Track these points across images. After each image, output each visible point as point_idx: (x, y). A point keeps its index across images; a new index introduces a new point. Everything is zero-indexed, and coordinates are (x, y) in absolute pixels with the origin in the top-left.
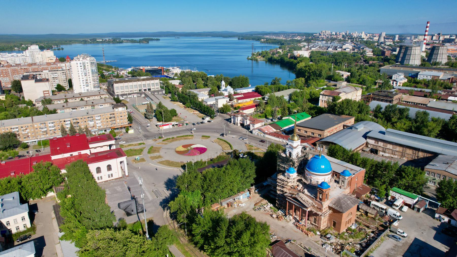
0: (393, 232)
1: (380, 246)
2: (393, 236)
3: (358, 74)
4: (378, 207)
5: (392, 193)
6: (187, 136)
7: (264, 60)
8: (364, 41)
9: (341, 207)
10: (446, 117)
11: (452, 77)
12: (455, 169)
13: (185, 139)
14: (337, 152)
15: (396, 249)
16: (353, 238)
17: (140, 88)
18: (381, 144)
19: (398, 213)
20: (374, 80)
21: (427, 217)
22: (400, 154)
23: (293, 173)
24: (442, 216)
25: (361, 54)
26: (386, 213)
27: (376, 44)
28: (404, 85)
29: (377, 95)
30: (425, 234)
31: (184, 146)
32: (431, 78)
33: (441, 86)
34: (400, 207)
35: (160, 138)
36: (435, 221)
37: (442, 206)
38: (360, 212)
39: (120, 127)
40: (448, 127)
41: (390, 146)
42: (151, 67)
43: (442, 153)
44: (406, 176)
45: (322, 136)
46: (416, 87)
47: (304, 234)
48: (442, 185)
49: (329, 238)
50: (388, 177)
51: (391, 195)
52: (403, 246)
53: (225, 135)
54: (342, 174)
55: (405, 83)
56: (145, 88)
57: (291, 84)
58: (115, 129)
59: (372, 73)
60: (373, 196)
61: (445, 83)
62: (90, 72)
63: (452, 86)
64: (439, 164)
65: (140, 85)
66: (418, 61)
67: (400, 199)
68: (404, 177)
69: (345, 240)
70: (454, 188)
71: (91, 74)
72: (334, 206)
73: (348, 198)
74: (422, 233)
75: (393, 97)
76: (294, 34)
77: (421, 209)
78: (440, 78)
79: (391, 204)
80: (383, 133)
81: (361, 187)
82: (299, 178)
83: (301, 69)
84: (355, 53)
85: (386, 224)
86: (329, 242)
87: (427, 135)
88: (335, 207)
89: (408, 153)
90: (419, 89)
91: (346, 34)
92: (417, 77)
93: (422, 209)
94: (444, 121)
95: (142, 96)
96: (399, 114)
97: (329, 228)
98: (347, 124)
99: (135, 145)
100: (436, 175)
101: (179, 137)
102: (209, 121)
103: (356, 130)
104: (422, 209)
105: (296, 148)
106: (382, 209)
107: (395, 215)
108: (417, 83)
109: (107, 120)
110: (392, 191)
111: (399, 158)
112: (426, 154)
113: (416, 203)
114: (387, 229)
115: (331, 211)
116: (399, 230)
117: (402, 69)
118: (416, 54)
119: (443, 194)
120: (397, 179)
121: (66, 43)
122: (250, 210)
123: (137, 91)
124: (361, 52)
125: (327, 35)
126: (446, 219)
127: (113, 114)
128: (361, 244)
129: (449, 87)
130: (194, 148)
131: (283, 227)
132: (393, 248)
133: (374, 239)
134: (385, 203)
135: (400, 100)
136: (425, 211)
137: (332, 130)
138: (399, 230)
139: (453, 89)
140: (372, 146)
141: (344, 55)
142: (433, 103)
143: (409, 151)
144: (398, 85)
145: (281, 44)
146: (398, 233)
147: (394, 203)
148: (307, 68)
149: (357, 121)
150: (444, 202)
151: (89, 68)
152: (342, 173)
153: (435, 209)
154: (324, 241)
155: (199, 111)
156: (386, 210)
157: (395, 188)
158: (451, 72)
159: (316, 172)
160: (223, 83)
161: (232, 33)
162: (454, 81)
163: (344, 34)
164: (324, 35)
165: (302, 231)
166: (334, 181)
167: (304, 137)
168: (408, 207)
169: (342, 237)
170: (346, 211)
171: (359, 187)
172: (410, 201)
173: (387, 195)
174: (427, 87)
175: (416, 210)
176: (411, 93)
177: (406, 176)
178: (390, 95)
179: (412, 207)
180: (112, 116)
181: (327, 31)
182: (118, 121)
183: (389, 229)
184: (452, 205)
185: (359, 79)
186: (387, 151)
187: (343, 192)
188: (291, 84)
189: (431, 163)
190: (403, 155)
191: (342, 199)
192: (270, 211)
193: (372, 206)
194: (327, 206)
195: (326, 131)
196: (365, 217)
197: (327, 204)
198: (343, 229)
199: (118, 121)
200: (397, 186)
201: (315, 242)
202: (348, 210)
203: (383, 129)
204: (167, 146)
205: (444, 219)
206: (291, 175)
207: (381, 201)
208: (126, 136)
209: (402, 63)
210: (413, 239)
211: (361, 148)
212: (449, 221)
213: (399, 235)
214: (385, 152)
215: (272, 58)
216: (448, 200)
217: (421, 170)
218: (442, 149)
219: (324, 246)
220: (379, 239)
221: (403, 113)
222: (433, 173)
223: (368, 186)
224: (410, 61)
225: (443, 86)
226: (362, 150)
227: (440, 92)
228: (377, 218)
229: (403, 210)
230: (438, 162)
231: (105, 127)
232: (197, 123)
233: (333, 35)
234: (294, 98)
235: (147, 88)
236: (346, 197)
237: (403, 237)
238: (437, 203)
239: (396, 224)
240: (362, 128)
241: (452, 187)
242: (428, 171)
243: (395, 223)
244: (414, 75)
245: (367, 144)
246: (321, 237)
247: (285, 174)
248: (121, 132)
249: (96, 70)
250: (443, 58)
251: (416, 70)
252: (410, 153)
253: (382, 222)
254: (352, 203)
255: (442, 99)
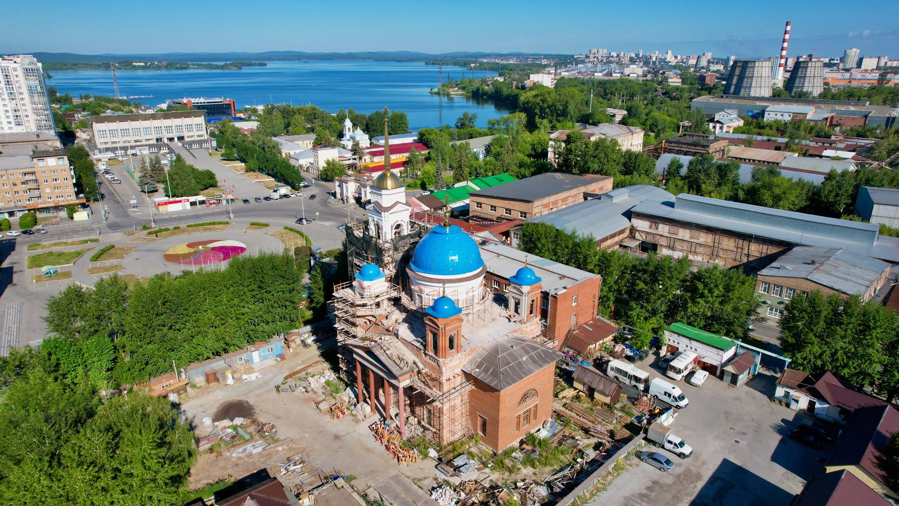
0: (653, 443)
1: (609, 488)
2: (652, 456)
3: (646, 111)
4: (625, 374)
5: (669, 338)
6: (214, 223)
7: (462, 95)
8: (671, 66)
9: (495, 374)
10: (818, 180)
11: (832, 115)
12: (831, 275)
13: (206, 229)
14: (539, 239)
15: (653, 495)
16: (533, 466)
17: (159, 136)
18: (664, 229)
19: (677, 388)
20: (676, 121)
21: (754, 398)
22: (708, 251)
23: (371, 280)
24: (793, 393)
25: (660, 83)
26: (647, 390)
27: (692, 70)
28: (737, 130)
29: (675, 143)
30: (743, 443)
31: (190, 246)
32: (790, 118)
33: (810, 133)
34: (685, 373)
35: (145, 228)
36: (775, 406)
37: (794, 365)
38: (575, 389)
39: (53, 205)
40: (821, 197)
41: (684, 234)
42: (206, 99)
43: (802, 243)
44: (706, 292)
45: (528, 215)
46: (759, 134)
47: (392, 455)
48: (795, 308)
49: (457, 469)
50: (663, 296)
51: (667, 342)
52: (675, 483)
53: (304, 222)
54: (514, 280)
55: (739, 127)
56: (171, 136)
57: (496, 126)
58: (41, 210)
59: (674, 110)
60: (619, 348)
61: (818, 128)
62: (25, 90)
63: (832, 132)
64: (793, 266)
65: (158, 128)
66: (767, 90)
67: (688, 353)
68: (702, 295)
69: (507, 473)
70: (824, 313)
71: (26, 96)
72: (476, 372)
73: (523, 348)
74: (737, 442)
75: (708, 146)
76: (537, 55)
77: (741, 377)
78: (808, 118)
79: (663, 366)
80: (671, 205)
81: (588, 325)
82: (394, 294)
83: (528, 102)
84: (647, 80)
85: (640, 422)
86: (456, 481)
87: (772, 207)
88: (480, 374)
89: (726, 247)
90: (765, 138)
91: (637, 55)
92: (763, 117)
93: (743, 378)
94: (811, 186)
95: (162, 152)
96: (717, 176)
97: (471, 437)
98: (594, 191)
99: (73, 244)
100: (784, 290)
101: (191, 226)
102: (286, 196)
103: (609, 201)
104: (743, 378)
105: (388, 209)
106: (637, 379)
107: (670, 395)
108: (763, 127)
109: (16, 189)
110: (669, 331)
111: (705, 260)
112: (765, 247)
113: (729, 361)
114: (637, 434)
115: (470, 387)
116: (671, 438)
117: (734, 102)
118: (763, 75)
119: (797, 336)
120: (685, 303)
121: (65, 67)
122: (267, 391)
123: (151, 142)
124: (660, 79)
125: (600, 58)
126: (803, 401)
127: (33, 173)
128: (549, 485)
129: (825, 134)
130: (214, 249)
131: (337, 437)
132: (645, 492)
133: (595, 464)
134: (652, 366)
135: (723, 154)
136: (753, 383)
137: (555, 203)
138: (670, 438)
139: (833, 138)
140: (644, 236)
141: (625, 82)
142: (791, 160)
143: (728, 243)
144: (724, 131)
145: (502, 70)
146: (667, 446)
147: (672, 363)
148: (538, 100)
149: (616, 186)
150: (799, 356)
151: (22, 83)
152: (514, 277)
153: (778, 375)
154: (442, 477)
155: (273, 177)
156: (646, 381)
157: (675, 326)
158: (830, 107)
159: (430, 272)
160: (348, 123)
161: (416, 54)
162: (834, 123)
163: (634, 55)
164: (595, 57)
165: (387, 448)
166: (491, 296)
167: (491, 220)
168: (707, 373)
169: (500, 465)
170: (509, 384)
171: (586, 324)
172: (714, 358)
173: (656, 344)
174: (782, 135)
175: (727, 378)
176: (749, 144)
177: (706, 292)
178: (702, 142)
179: (718, 373)
180: (28, 177)
181: (600, 50)
182: (48, 190)
183: (642, 435)
184: (819, 363)
185: (646, 120)
186: (678, 245)
187: (515, 331)
188: (496, 126)
189: (774, 264)
190: (715, 253)
191: (505, 349)
192: (320, 391)
193: (611, 373)
194: (458, 371)
195: (537, 203)
196: (586, 404)
197: (458, 365)
198: (509, 439)
199: (48, 190)
200: (685, 321)
201: (413, 480)
202: (515, 381)
203: (672, 198)
204: (151, 246)
205: (797, 401)
206: (366, 283)
207: (641, 358)
208: (68, 225)
209: (737, 93)
210: (718, 462)
211: (617, 239)
212: (811, 405)
213: (669, 451)
214: (672, 248)
215: (478, 89)
216: (808, 349)
217: (744, 272)
218: (801, 234)
219: (435, 495)
220: (610, 465)
221: (726, 174)
222: (778, 286)
223: (613, 324)
224: (752, 89)
225: (814, 132)
226: (621, 246)
227: (808, 142)
228: (618, 406)
229: (693, 380)
230: (789, 262)
231: (12, 204)
232: (257, 199)
233: (613, 57)
234: (495, 149)
235: (175, 135)
236: (518, 344)
237: (681, 455)
238: (781, 358)
239: (666, 420)
240: (624, 198)
241: (820, 312)
242: (766, 283)
243: (664, 417)
244: (758, 114)
245: (633, 230)
246: (436, 467)
247: (354, 283)
248: (56, 217)
249: (39, 88)
250: (815, 85)
251: (762, 104)
252: (729, 248)
253: (631, 415)
254: (534, 361)
255: (811, 156)
